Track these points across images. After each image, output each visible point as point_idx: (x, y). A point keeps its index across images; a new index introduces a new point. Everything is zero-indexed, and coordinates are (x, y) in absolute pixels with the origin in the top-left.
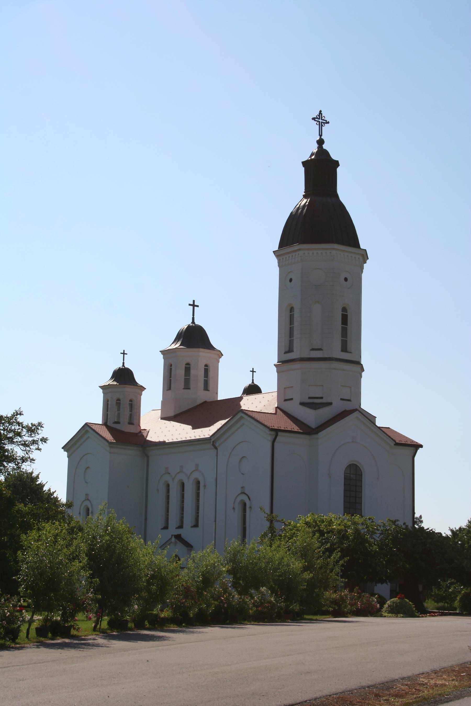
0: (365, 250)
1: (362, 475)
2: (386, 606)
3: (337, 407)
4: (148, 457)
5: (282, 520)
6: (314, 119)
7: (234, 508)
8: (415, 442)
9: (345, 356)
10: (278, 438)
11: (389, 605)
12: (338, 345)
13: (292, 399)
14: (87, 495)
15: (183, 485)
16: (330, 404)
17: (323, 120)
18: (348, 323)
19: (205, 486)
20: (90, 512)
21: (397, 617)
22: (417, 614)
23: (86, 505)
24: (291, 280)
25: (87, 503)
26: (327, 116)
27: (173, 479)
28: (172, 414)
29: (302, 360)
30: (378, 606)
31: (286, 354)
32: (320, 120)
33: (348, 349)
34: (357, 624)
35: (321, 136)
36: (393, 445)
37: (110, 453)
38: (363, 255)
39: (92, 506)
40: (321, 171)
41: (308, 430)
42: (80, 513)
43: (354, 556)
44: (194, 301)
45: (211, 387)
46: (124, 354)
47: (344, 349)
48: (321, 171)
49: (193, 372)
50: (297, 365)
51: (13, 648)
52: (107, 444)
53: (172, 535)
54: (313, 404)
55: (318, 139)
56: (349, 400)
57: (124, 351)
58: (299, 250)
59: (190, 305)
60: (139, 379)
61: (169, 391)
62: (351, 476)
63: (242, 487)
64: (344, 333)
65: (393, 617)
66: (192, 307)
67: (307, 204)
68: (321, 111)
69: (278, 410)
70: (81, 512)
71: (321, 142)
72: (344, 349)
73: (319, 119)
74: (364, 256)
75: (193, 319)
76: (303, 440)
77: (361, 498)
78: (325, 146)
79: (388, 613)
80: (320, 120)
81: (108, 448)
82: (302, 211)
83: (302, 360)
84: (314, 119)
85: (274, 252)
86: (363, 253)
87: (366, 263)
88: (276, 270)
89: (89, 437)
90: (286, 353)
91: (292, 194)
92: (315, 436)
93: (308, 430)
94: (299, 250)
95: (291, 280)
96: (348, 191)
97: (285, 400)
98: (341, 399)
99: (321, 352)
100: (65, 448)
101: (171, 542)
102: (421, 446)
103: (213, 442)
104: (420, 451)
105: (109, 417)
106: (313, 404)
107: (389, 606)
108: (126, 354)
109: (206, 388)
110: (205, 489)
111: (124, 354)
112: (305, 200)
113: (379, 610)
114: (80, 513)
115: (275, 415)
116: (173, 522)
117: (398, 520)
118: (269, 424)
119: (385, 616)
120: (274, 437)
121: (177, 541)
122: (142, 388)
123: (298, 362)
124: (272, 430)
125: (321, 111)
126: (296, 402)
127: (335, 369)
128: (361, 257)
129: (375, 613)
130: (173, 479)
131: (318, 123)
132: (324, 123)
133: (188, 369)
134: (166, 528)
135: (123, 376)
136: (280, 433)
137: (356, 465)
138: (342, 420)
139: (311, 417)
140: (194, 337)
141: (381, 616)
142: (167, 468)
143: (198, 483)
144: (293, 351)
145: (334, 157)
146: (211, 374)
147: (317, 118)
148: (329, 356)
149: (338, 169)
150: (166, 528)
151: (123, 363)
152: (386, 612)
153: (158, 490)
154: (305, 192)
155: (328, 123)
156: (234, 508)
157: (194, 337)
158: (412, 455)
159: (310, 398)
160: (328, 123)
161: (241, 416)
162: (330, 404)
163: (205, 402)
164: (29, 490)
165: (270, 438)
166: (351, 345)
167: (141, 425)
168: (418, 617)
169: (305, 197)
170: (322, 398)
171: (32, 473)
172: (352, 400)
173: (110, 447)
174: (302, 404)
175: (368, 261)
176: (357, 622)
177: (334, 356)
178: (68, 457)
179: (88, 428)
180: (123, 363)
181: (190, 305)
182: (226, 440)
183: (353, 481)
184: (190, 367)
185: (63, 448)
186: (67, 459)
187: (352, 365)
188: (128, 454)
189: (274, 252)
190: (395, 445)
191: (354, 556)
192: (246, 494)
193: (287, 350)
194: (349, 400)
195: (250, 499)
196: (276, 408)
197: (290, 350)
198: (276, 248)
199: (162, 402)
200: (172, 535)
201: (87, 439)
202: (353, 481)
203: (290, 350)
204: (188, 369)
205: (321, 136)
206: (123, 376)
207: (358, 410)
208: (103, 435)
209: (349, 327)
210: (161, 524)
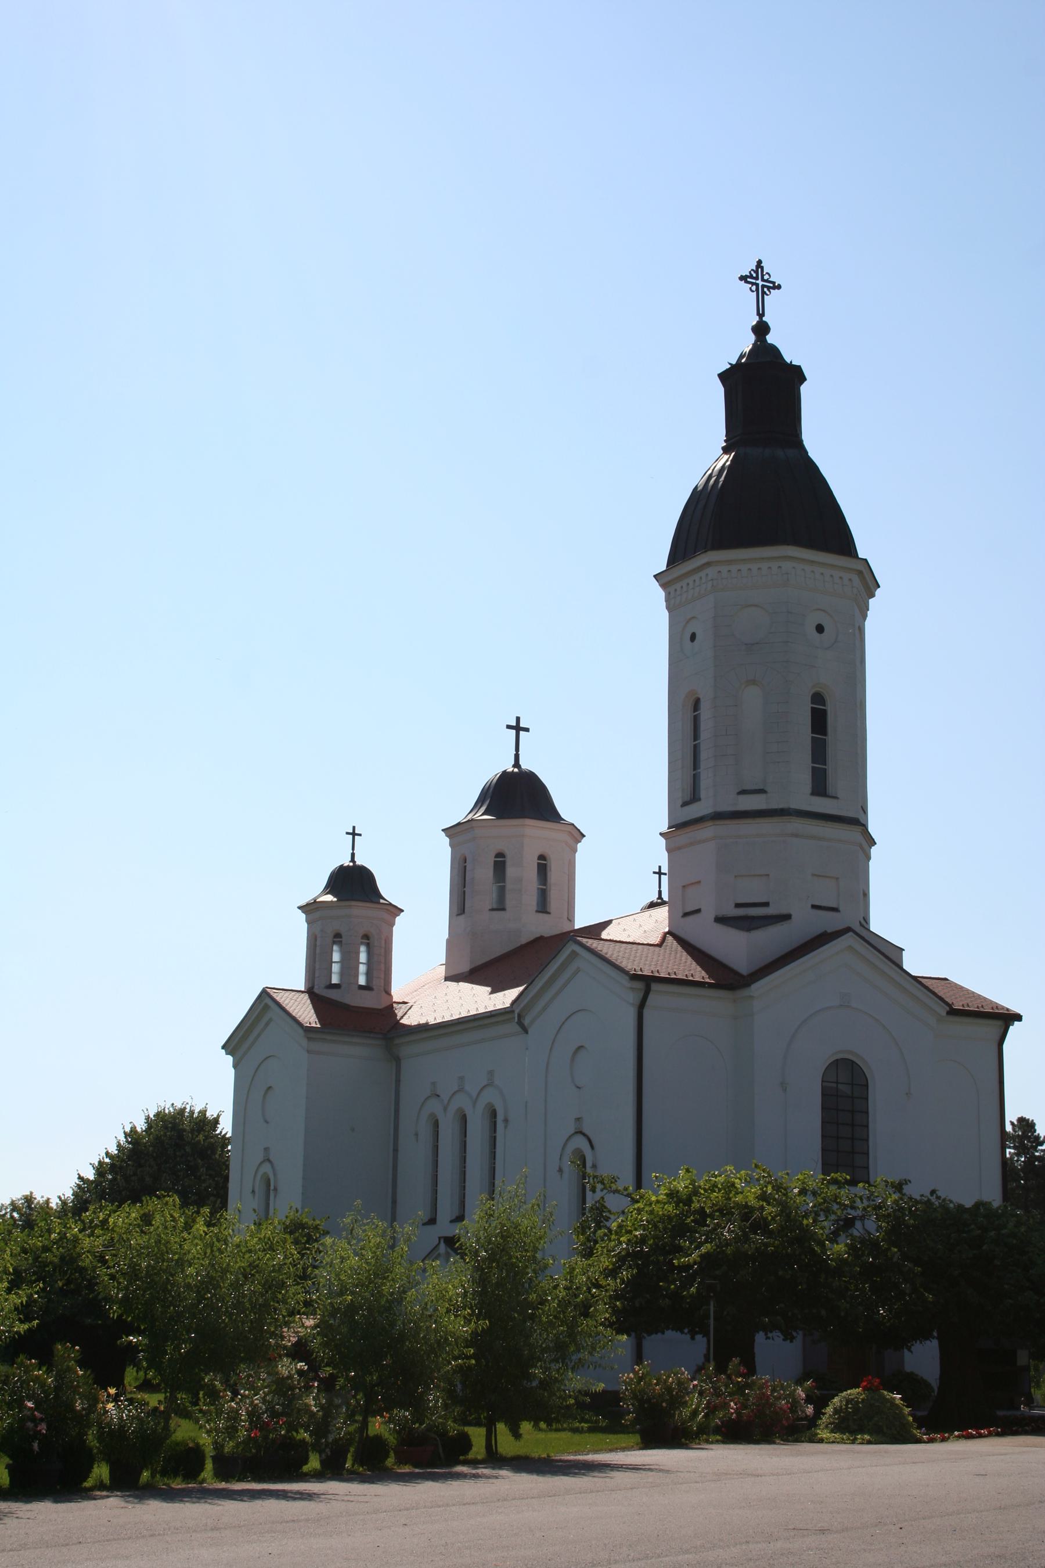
0: (866, 560)
1: (867, 1086)
2: (829, 1410)
3: (805, 923)
4: (397, 1060)
5: (626, 1189)
6: (743, 278)
7: (560, 1170)
8: (1003, 1008)
9: (820, 805)
10: (652, 997)
11: (835, 1409)
12: (803, 778)
13: (698, 911)
14: (266, 1149)
15: (464, 1119)
16: (787, 917)
17: (767, 281)
18: (828, 732)
19: (506, 1121)
20: (272, 1187)
21: (853, 1442)
22: (917, 1433)
23: (265, 1173)
24: (693, 637)
25: (266, 1168)
26: (774, 271)
27: (445, 1109)
28: (465, 968)
29: (718, 816)
30: (810, 1410)
31: (686, 808)
32: (760, 282)
33: (830, 791)
34: (650, 1477)
35: (761, 315)
36: (944, 1014)
37: (308, 1052)
38: (860, 573)
39: (275, 1174)
40: (763, 392)
41: (726, 979)
42: (253, 1191)
43: (780, 1273)
44: (518, 719)
45: (554, 904)
46: (354, 834)
47: (820, 787)
48: (763, 392)
49: (510, 871)
50: (708, 831)
51: (358, 1474)
52: (301, 1031)
53: (440, 1238)
54: (745, 919)
55: (754, 323)
56: (835, 910)
57: (354, 828)
58: (708, 564)
59: (509, 727)
60: (388, 889)
61: (462, 917)
62: (840, 1086)
63: (578, 1119)
64: (819, 752)
65: (842, 1442)
66: (514, 731)
67: (728, 463)
68: (760, 262)
69: (670, 938)
70: (257, 1190)
71: (761, 329)
72: (820, 787)
73: (763, 286)
74: (868, 583)
75: (517, 757)
76: (719, 1003)
77: (867, 1140)
78: (770, 339)
79: (832, 1431)
80: (760, 282)
81: (304, 1042)
82: (717, 481)
83: (718, 816)
84: (743, 278)
85: (655, 576)
86: (860, 567)
87: (873, 595)
88: (661, 619)
89: (271, 1020)
90: (685, 804)
91: (698, 446)
92: (745, 992)
93: (726, 979)
94: (708, 564)
95: (693, 637)
96: (827, 433)
97: (686, 915)
98: (814, 907)
99: (762, 796)
100: (223, 1047)
101: (439, 1255)
102: (1018, 1018)
103: (519, 1016)
104: (1015, 1030)
105: (317, 975)
106: (745, 919)
107: (836, 1411)
108: (360, 835)
109: (543, 907)
110: (506, 1127)
111: (354, 834)
112: (726, 457)
113: (812, 1422)
114: (253, 1191)
115: (657, 949)
116: (446, 1210)
117: (907, 1182)
118: (629, 966)
119: (821, 1441)
120: (641, 995)
121: (449, 1250)
122: (393, 909)
123: (710, 823)
124: (635, 977)
125: (760, 262)
126: (709, 914)
127: (797, 836)
128: (856, 579)
129: (794, 1430)
130: (445, 1109)
131: (754, 288)
132: (769, 288)
133: (500, 865)
134: (432, 1221)
135: (353, 883)
136: (654, 987)
137: (853, 1062)
138: (811, 954)
139: (736, 948)
140: (516, 796)
141: (813, 1439)
142: (434, 1084)
143: (494, 1114)
144: (700, 799)
145: (790, 356)
146: (553, 876)
147: (751, 277)
148: (781, 806)
149: (804, 389)
150: (432, 1221)
151: (353, 855)
152: (827, 1427)
153: (416, 1135)
154: (725, 441)
155: (779, 287)
156: (560, 1170)
157: (516, 796)
158: (997, 1038)
159: (738, 905)
160: (779, 287)
161: (573, 952)
162: (787, 917)
163: (540, 939)
164: (188, 1149)
165: (633, 998)
166: (837, 781)
167: (393, 993)
168: (918, 1441)
169: (726, 450)
170: (766, 904)
171: (203, 1112)
172: (841, 909)
173: (309, 1039)
174: (720, 920)
175: (878, 592)
176: (635, 1468)
177: (794, 805)
178: (235, 1066)
179: (268, 1001)
180: (353, 855)
181: (509, 727)
182: (545, 1008)
183: (845, 1104)
184: (504, 862)
185: (223, 1047)
186: (233, 1071)
187: (837, 825)
188: (352, 1055)
189: (655, 576)
190: (948, 1013)
191: (780, 1273)
192: (584, 1135)
193: (687, 798)
194: (835, 910)
195: (592, 1147)
196: (666, 934)
197: (694, 797)
198: (663, 567)
199: (448, 941)
200: (440, 1238)
201: (267, 1024)
202: (845, 1104)
203: (694, 797)
204: (500, 865)
205: (761, 315)
206: (353, 883)
207: (859, 930)
208: (291, 1010)
209: (830, 738)
210: (422, 1214)
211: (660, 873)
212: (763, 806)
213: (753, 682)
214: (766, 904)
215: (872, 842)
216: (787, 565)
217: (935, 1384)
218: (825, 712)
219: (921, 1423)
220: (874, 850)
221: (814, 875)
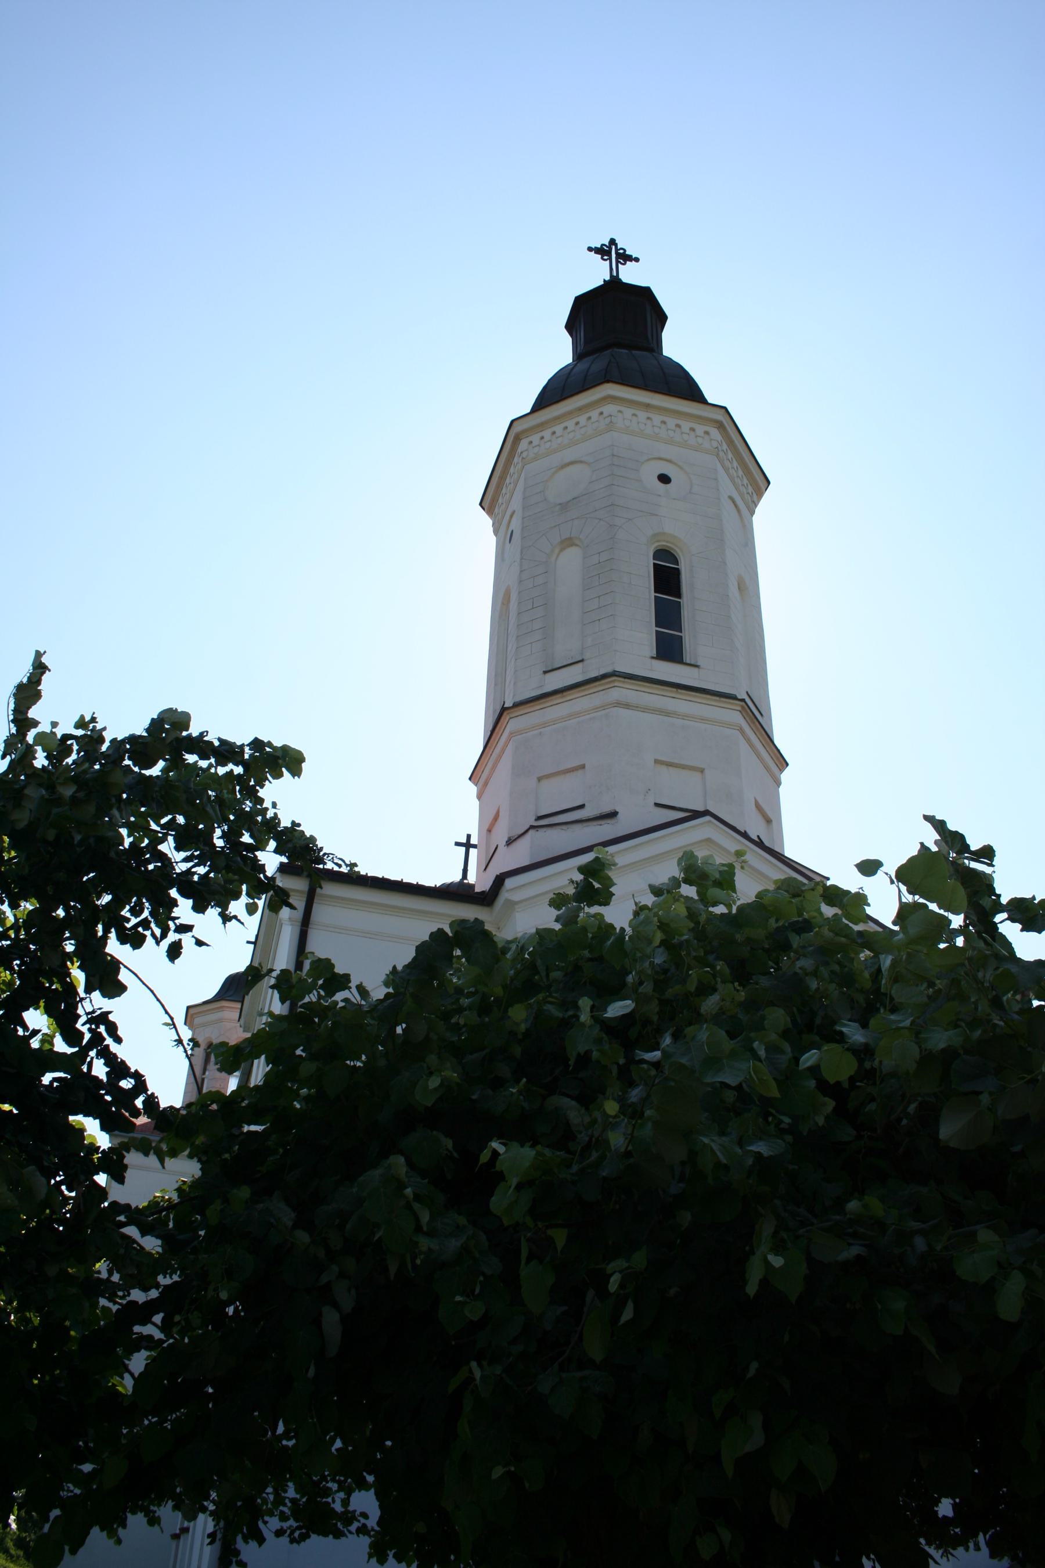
33: (687, 658)
38: (720, 426)
47: (669, 649)
72: (669, 649)
98: (657, 805)
127: (627, 706)
128: (715, 433)
170: (582, 806)
211: (468, 845)
212: (580, 678)
213: (568, 542)
214: (582, 806)
215: (783, 763)
216: (609, 409)
217: (105, 1080)
218: (677, 572)
219: (20, 1543)
220: (785, 776)
221: (657, 761)
